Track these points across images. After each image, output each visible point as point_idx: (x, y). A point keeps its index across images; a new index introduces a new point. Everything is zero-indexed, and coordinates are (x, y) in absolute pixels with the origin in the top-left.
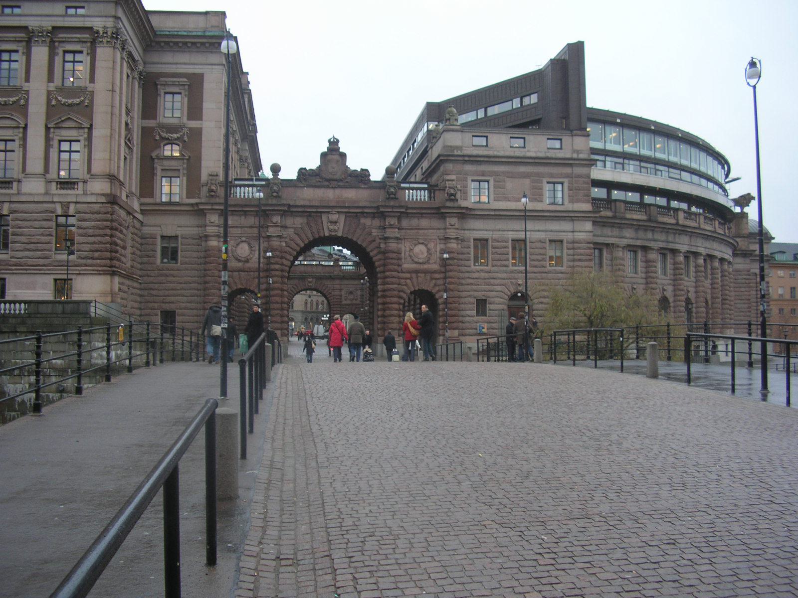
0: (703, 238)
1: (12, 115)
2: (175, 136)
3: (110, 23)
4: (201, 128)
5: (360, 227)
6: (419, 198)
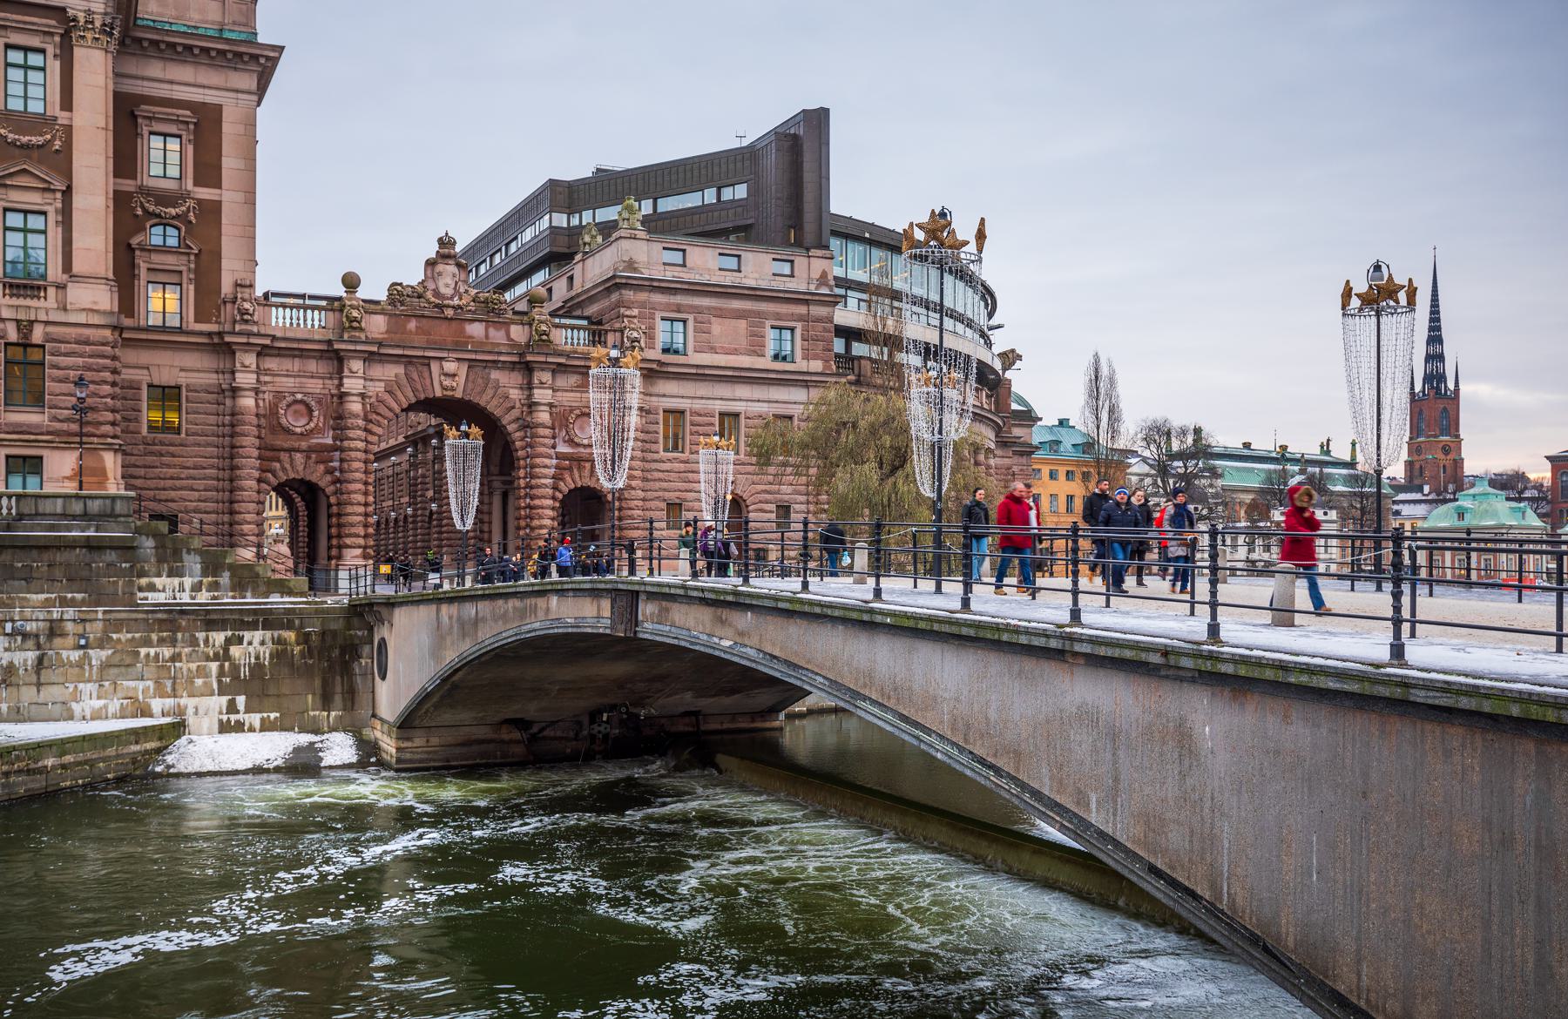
2: (173, 211)
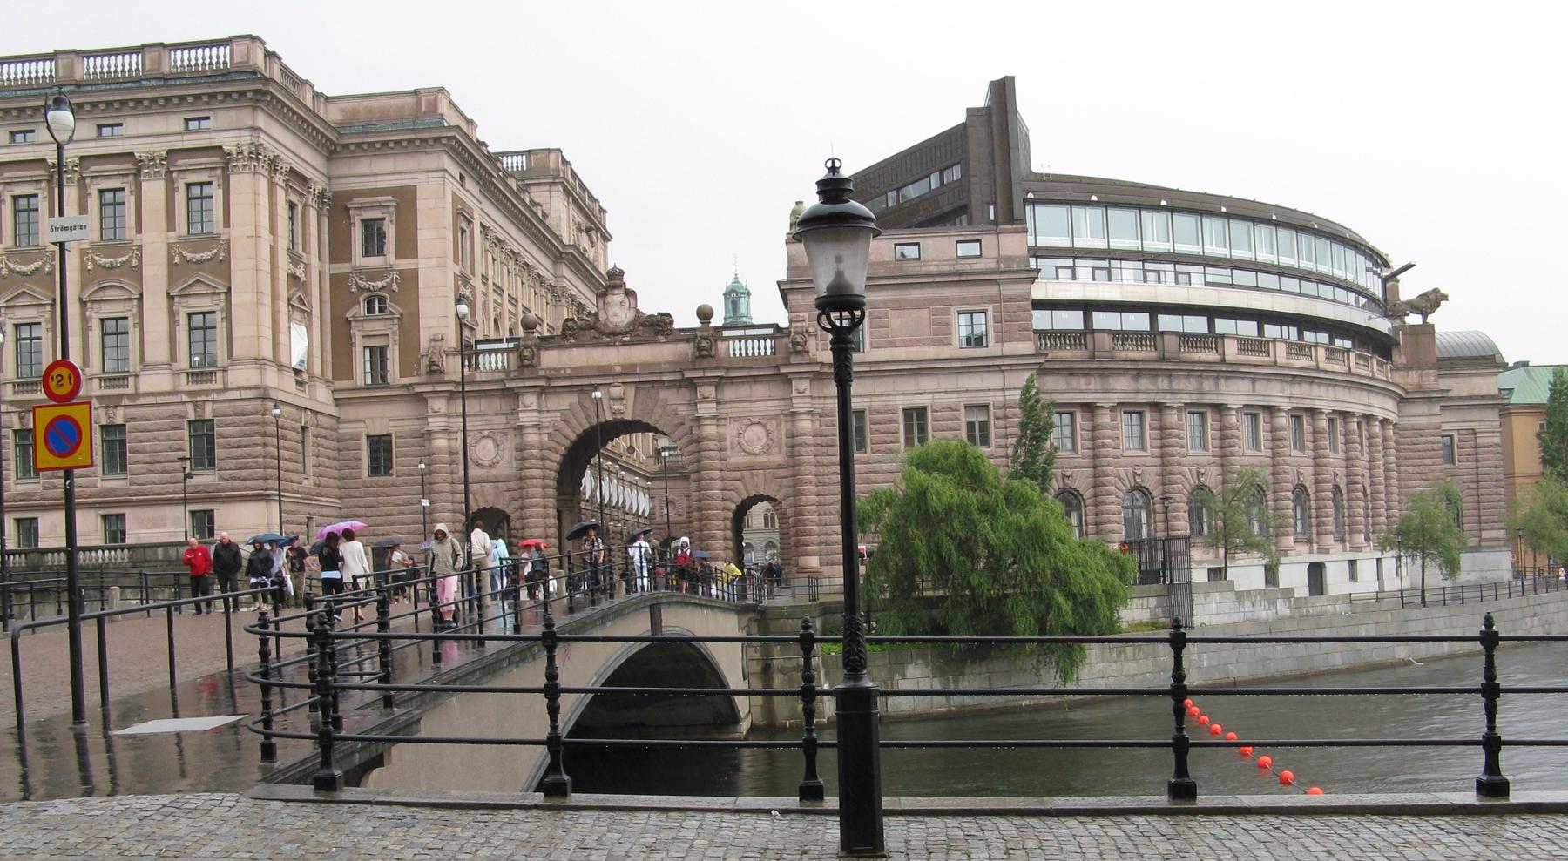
0: (1345, 387)
1: (121, 282)
3: (246, 138)
5: (659, 403)
6: (762, 351)
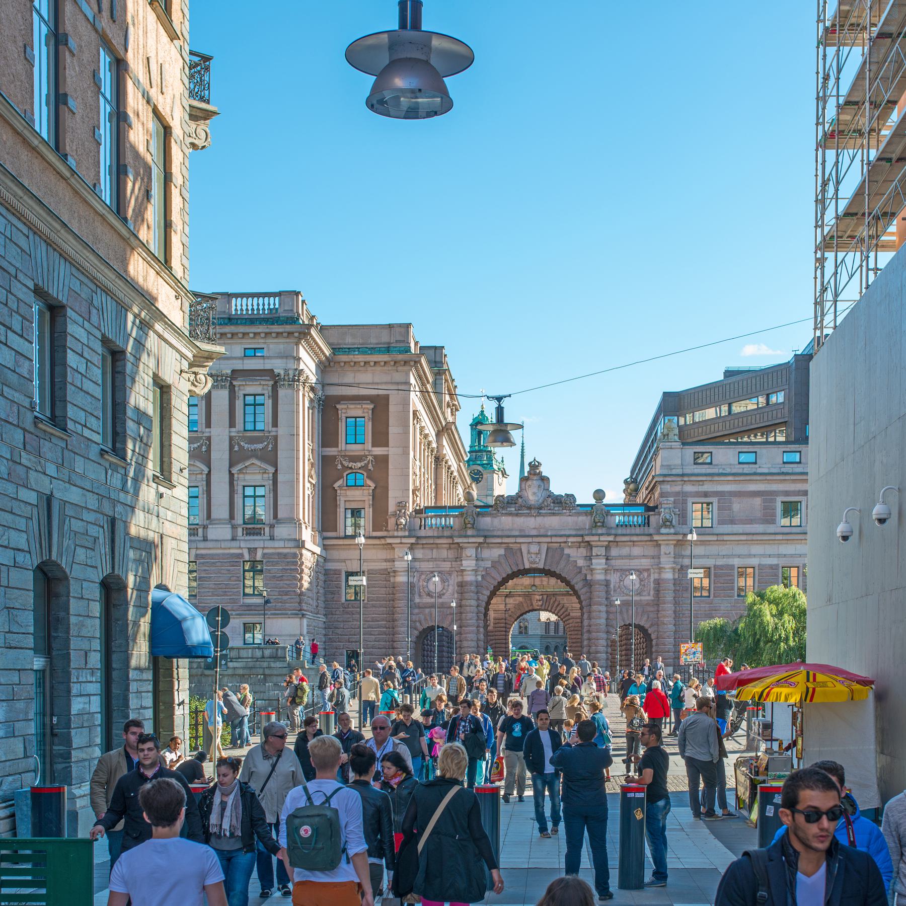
4: (388, 455)
